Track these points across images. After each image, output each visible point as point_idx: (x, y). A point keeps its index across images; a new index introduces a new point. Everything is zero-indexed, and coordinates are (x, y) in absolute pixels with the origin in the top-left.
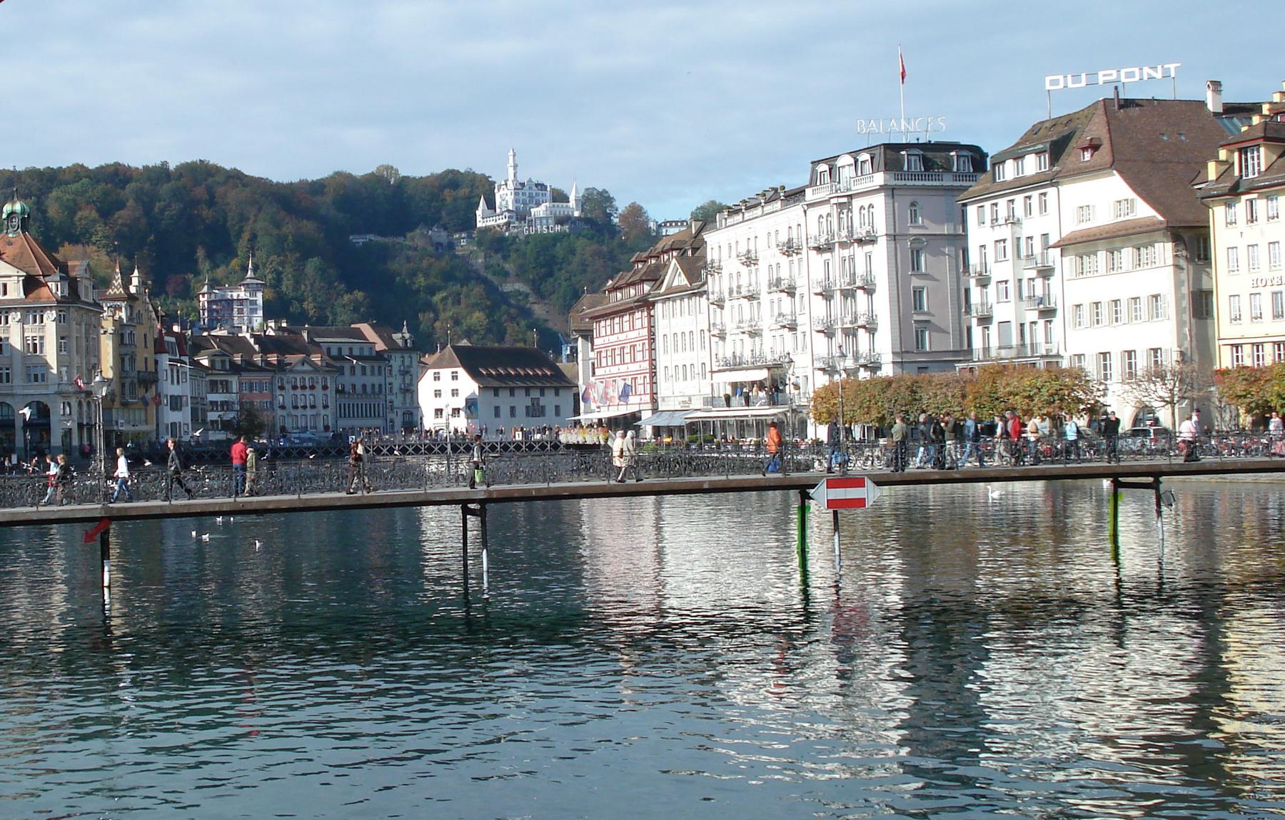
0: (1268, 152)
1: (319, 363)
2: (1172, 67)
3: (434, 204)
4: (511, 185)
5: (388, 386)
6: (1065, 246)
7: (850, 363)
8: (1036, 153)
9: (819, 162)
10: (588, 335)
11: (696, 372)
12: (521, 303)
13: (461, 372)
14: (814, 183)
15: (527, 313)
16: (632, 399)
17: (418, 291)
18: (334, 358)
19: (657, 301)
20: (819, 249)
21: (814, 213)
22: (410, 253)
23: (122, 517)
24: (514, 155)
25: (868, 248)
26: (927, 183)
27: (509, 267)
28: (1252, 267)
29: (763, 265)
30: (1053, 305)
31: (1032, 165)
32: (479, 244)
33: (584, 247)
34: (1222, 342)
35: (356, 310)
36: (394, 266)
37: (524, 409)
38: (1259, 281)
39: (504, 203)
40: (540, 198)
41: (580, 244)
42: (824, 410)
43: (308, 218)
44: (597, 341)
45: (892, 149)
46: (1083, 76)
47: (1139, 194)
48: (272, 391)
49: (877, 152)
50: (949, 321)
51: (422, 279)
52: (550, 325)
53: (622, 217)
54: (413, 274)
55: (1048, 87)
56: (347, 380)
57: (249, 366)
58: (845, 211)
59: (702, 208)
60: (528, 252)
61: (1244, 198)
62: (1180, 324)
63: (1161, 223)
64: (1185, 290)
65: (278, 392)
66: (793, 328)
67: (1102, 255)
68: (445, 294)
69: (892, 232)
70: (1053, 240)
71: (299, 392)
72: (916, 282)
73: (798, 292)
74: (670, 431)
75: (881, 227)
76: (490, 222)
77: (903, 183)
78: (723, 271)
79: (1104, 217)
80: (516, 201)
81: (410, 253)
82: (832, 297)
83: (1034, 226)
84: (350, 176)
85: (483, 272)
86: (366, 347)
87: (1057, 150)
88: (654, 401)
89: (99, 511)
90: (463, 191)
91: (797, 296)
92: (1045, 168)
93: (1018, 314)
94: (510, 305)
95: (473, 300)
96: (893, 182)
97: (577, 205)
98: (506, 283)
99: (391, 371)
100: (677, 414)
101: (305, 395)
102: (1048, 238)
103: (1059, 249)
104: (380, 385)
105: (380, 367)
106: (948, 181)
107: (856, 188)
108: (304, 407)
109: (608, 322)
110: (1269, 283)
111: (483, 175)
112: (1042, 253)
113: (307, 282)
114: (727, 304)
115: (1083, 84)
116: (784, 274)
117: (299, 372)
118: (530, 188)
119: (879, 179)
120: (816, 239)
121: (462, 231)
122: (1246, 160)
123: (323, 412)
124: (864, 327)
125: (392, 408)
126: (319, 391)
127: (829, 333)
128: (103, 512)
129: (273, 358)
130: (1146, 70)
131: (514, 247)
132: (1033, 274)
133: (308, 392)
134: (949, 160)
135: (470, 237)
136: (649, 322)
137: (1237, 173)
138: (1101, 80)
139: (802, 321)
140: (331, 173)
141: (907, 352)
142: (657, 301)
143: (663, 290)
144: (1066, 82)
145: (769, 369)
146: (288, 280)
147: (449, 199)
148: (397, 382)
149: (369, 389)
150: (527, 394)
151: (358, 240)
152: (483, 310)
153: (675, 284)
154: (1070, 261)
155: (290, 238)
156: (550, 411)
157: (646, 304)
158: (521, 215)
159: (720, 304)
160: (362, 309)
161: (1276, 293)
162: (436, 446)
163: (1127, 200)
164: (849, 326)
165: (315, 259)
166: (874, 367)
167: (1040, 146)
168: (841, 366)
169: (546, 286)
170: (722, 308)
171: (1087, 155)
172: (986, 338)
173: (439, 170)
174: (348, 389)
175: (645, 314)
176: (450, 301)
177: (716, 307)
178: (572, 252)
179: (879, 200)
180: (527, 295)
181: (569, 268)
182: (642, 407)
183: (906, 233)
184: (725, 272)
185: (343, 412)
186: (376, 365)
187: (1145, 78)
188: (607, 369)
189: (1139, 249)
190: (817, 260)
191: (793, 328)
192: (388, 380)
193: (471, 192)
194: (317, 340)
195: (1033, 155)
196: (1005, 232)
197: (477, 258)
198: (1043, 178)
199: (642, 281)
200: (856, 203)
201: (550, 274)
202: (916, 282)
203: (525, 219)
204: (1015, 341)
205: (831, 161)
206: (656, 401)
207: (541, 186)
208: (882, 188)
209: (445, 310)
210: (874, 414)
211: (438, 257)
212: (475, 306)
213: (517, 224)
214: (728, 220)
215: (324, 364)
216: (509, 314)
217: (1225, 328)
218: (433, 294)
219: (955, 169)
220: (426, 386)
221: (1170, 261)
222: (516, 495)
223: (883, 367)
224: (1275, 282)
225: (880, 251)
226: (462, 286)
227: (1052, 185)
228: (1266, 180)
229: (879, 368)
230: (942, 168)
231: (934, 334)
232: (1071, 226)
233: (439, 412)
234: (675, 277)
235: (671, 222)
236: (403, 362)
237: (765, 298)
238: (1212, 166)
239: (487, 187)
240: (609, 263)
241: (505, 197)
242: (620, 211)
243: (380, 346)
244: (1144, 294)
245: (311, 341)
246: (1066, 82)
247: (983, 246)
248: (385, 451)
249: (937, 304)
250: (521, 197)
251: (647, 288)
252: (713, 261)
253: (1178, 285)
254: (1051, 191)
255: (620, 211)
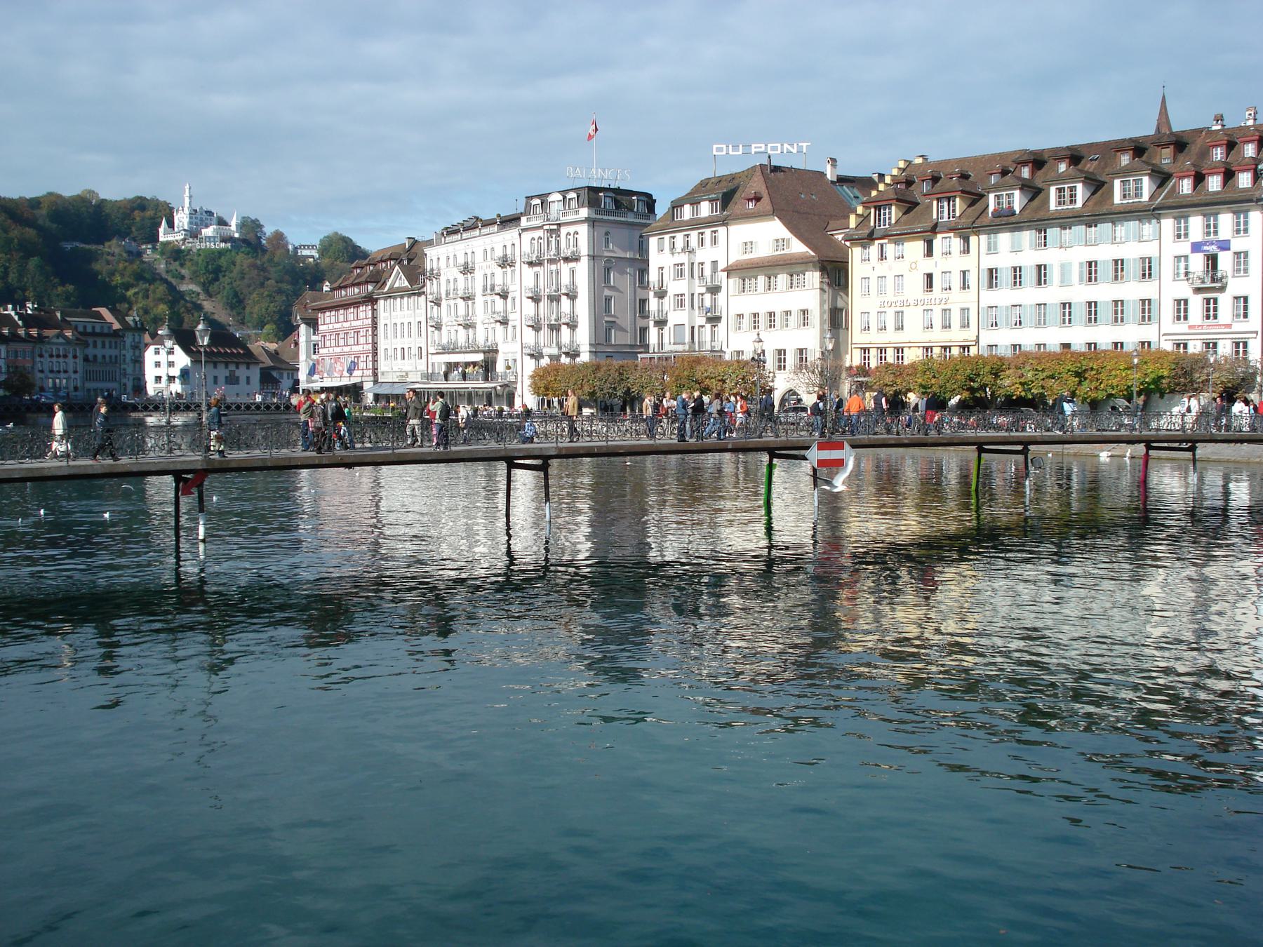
0: (1022, 196)
1: (70, 337)
2: (805, 145)
3: (126, 221)
4: (187, 211)
5: (122, 357)
6: (730, 271)
7: (555, 351)
8: (710, 201)
9: (532, 197)
10: (313, 324)
11: (389, 354)
12: (194, 300)
13: (177, 348)
14: (528, 213)
15: (199, 308)
16: (356, 373)
17: (116, 287)
18: (80, 333)
19: (379, 298)
20: (531, 264)
21: (527, 236)
22: (110, 258)
23: (223, 469)
24: (190, 188)
25: (572, 265)
26: (619, 219)
27: (184, 272)
28: (881, 291)
29: (478, 275)
30: (718, 314)
31: (705, 209)
32: (162, 253)
33: (243, 260)
34: (853, 346)
35: (67, 299)
36: (97, 266)
37: (245, 379)
38: (933, 301)
39: (181, 224)
40: (208, 222)
41: (239, 258)
42: (543, 385)
43: (30, 226)
44: (321, 328)
45: (593, 190)
46: (741, 146)
47: (795, 236)
48: (33, 358)
49: (582, 192)
50: (627, 324)
51: (119, 278)
52: (216, 317)
53: (268, 240)
54: (112, 274)
55: (715, 153)
56: (90, 351)
57: (14, 337)
58: (554, 236)
59: (328, 237)
60: (200, 261)
61: (877, 242)
62: (822, 331)
63: (813, 256)
64: (826, 307)
65: (38, 359)
66: (504, 322)
67: (761, 279)
68: (136, 290)
69: (592, 253)
70: (722, 265)
71: (55, 359)
72: (607, 292)
73: (510, 296)
74: (388, 398)
75: (584, 249)
76: (170, 238)
77: (600, 217)
78: (441, 277)
79: (764, 250)
80: (190, 223)
81: (110, 258)
82: (540, 300)
83: (705, 255)
84: (59, 196)
85: (164, 275)
86: (106, 326)
87: (727, 199)
88: (375, 374)
89: (200, 463)
90: (149, 213)
91: (509, 300)
92: (716, 212)
93: (691, 318)
94: (186, 301)
95: (158, 296)
96: (594, 216)
97: (237, 228)
98: (182, 284)
99: (124, 345)
100: (396, 385)
101: (59, 363)
102: (1013, 246)
103: (726, 273)
104: (116, 357)
105: (116, 342)
106: (631, 218)
107: (563, 219)
108: (59, 372)
109: (333, 313)
110: (894, 305)
111: (165, 202)
112: (712, 276)
113: (29, 276)
114: (444, 303)
115: (740, 153)
116: (498, 280)
117: (57, 344)
118: (201, 214)
119: (584, 212)
120: (528, 255)
121: (148, 243)
122: (880, 215)
123: (73, 376)
124: (567, 324)
125: (125, 374)
126: (70, 360)
127: (536, 327)
128: (205, 464)
129: (34, 332)
130: (786, 146)
131: (188, 257)
132: (703, 290)
133: (61, 360)
134: (632, 202)
135: (154, 248)
136: (373, 314)
137: (872, 223)
138: (753, 150)
139: (514, 318)
140: (45, 193)
141: (599, 344)
142: (379, 298)
143: (386, 289)
144: (728, 150)
145: (484, 352)
146: (14, 273)
147: (138, 219)
148: (129, 354)
149: (107, 359)
150: (227, 367)
151: (68, 246)
152: (166, 303)
153: (397, 285)
154: (734, 282)
155: (16, 241)
156: (243, 380)
157: (371, 300)
158: (193, 234)
159: (437, 303)
160: (72, 299)
161: (898, 312)
162: (155, 405)
163: (783, 240)
164: (553, 322)
165: (36, 258)
166: (574, 354)
167: (714, 196)
168: (546, 351)
169: (214, 288)
170: (439, 305)
171: (751, 205)
172: (661, 337)
173: (131, 196)
174: (91, 358)
175: (370, 307)
176: (141, 295)
177: (433, 304)
178: (234, 264)
179: (583, 229)
180: (198, 294)
181: (231, 275)
182: (366, 379)
183: (601, 254)
184: (443, 279)
185: (88, 376)
186: (113, 340)
187: (785, 152)
188: (331, 349)
189: (792, 276)
190: (529, 273)
191: (504, 322)
192: (123, 352)
193: (156, 214)
194: (68, 319)
195: (707, 203)
196: (683, 258)
197: (159, 264)
198: (716, 219)
199: (367, 282)
200: (564, 230)
201: (217, 279)
202: (607, 292)
203: (197, 237)
204: (687, 339)
205: (543, 197)
206: (377, 375)
207: (210, 213)
208: (587, 220)
209: (136, 302)
210: (587, 389)
211: (131, 262)
212: (161, 300)
213: (191, 240)
214: (447, 239)
215: (74, 338)
216: (186, 307)
217: (857, 336)
218: (127, 290)
219: (635, 210)
220: (150, 356)
221: (817, 285)
222: (582, 452)
223: (581, 354)
224: (898, 304)
225: (583, 268)
226: (150, 285)
227: (723, 225)
228: (897, 230)
229: (578, 355)
230: (627, 207)
231: (619, 333)
232: (736, 256)
233: (158, 379)
234: (397, 279)
235: (304, 246)
236: (134, 339)
237: (479, 299)
238: (852, 218)
239: (168, 211)
240: (262, 273)
241: (182, 219)
242: (267, 236)
243: (117, 326)
244: (795, 309)
245: (63, 320)
246: (728, 150)
247: (662, 268)
248: (151, 407)
249: (622, 310)
250: (194, 220)
251: (370, 288)
252: (432, 270)
253: (822, 303)
254: (722, 231)
255: (267, 236)
